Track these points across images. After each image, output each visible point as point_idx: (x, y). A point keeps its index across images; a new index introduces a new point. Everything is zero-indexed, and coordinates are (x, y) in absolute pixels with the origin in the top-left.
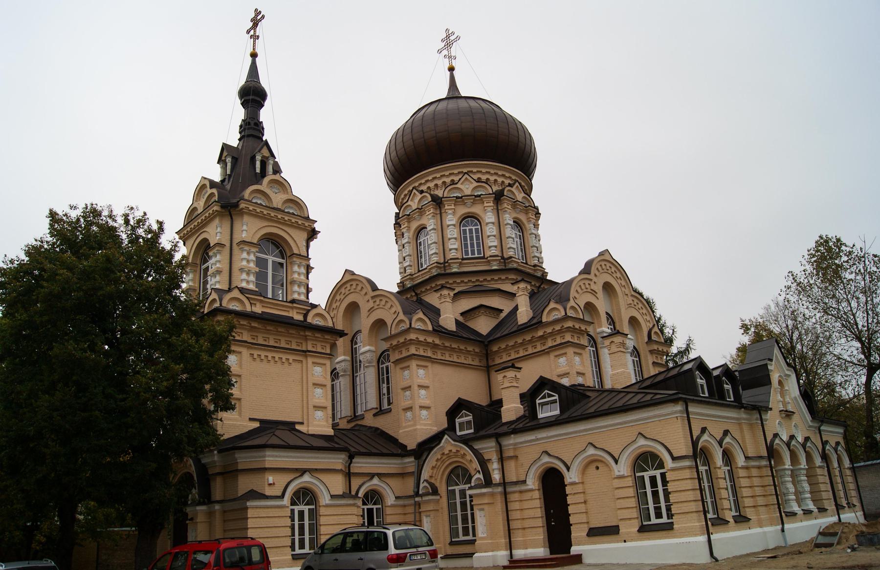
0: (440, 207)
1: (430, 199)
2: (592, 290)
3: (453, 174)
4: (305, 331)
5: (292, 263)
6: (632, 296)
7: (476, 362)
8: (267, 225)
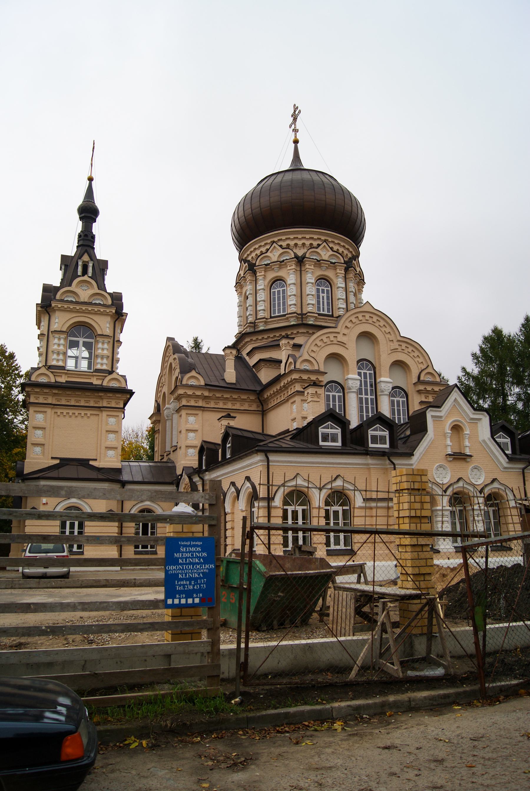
0: (301, 265)
1: (293, 256)
2: (338, 341)
3: (289, 238)
4: (98, 393)
5: (97, 342)
6: (398, 341)
7: (254, 407)
8: (75, 316)
